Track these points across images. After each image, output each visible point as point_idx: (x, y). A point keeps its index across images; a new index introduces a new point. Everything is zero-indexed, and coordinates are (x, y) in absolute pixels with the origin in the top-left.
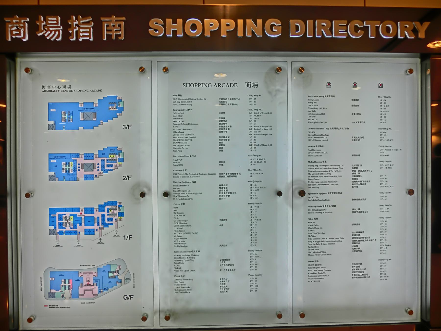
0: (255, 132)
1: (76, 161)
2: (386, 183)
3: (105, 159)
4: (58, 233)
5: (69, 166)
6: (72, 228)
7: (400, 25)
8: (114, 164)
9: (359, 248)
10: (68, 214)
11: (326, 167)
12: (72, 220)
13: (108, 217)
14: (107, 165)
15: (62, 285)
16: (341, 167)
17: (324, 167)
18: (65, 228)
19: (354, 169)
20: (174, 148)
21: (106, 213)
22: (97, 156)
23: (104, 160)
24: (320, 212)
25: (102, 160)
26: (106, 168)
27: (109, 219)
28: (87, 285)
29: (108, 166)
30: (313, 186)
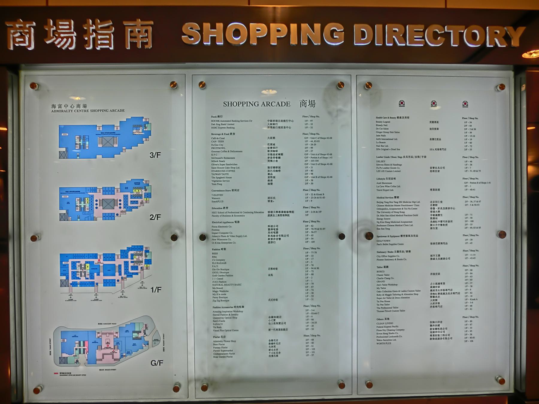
0: (312, 161)
1: (92, 196)
2: (472, 223)
3: (129, 194)
4: (71, 284)
5: (85, 203)
6: (87, 279)
7: (489, 31)
8: (139, 200)
9: (439, 303)
10: (83, 261)
11: (399, 204)
12: (89, 268)
13: (132, 264)
14: (131, 201)
15: (76, 347)
16: (416, 204)
17: (396, 204)
18: (80, 279)
19: (433, 207)
22: (119, 191)
23: (127, 196)
24: (391, 258)
25: (124, 196)
26: (130, 205)
27: (133, 268)
29: (132, 202)
30: (383, 227)
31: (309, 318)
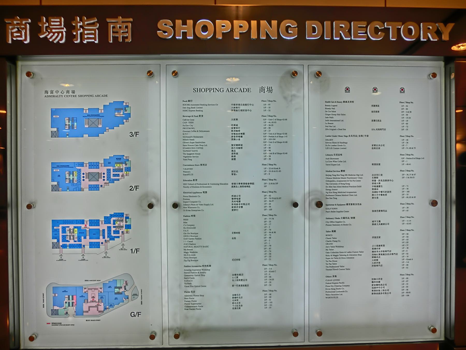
0: (270, 139)
1: (80, 170)
2: (408, 193)
3: (111, 168)
4: (61, 246)
5: (73, 176)
6: (76, 241)
7: (423, 27)
8: (121, 174)
10: (72, 226)
11: (345, 177)
12: (77, 232)
13: (114, 229)
14: (113, 174)
15: (66, 301)
16: (360, 176)
17: (342, 177)
18: (69, 241)
19: (374, 179)
20: (184, 157)
21: (112, 225)
22: (103, 165)
23: (110, 170)
24: (338, 224)
25: (107, 170)
26: (112, 177)
27: (115, 232)
28: (92, 301)
29: (114, 175)
30: (331, 197)
31: (267, 275)
